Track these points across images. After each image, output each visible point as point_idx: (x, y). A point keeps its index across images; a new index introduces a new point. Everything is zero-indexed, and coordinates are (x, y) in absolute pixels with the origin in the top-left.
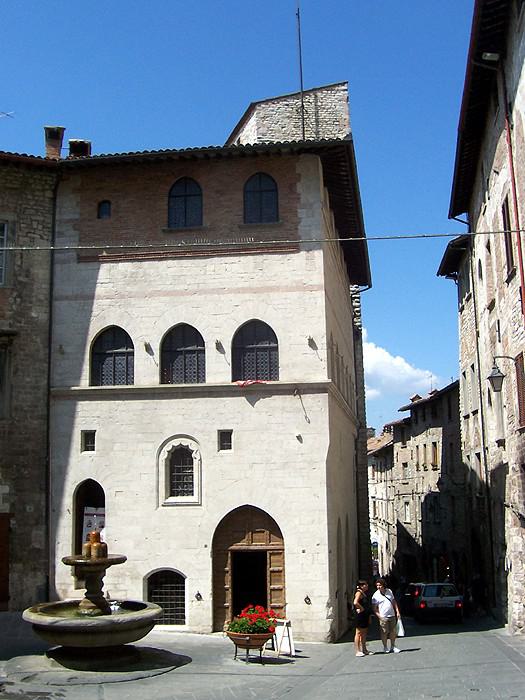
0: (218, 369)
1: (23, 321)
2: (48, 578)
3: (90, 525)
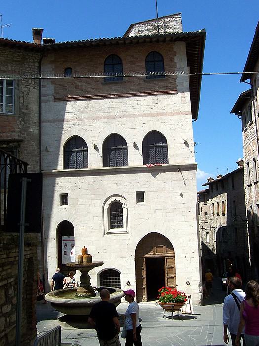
0: (135, 158)
1: (25, 134)
2: (44, 276)
3: (65, 246)
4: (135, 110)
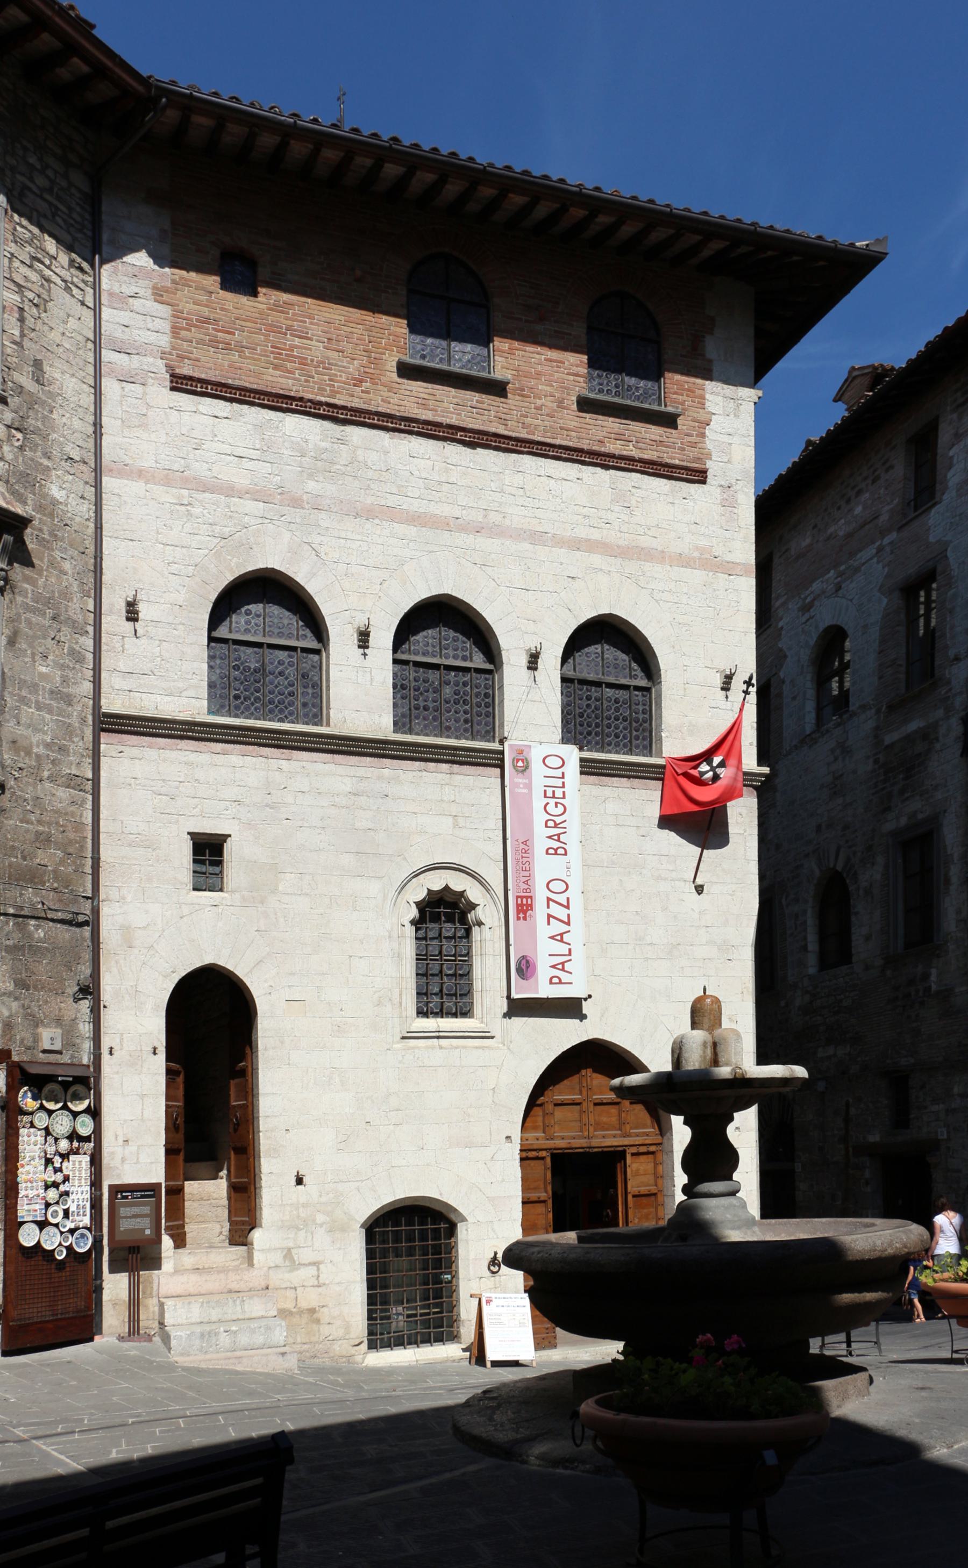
4: (539, 513)
